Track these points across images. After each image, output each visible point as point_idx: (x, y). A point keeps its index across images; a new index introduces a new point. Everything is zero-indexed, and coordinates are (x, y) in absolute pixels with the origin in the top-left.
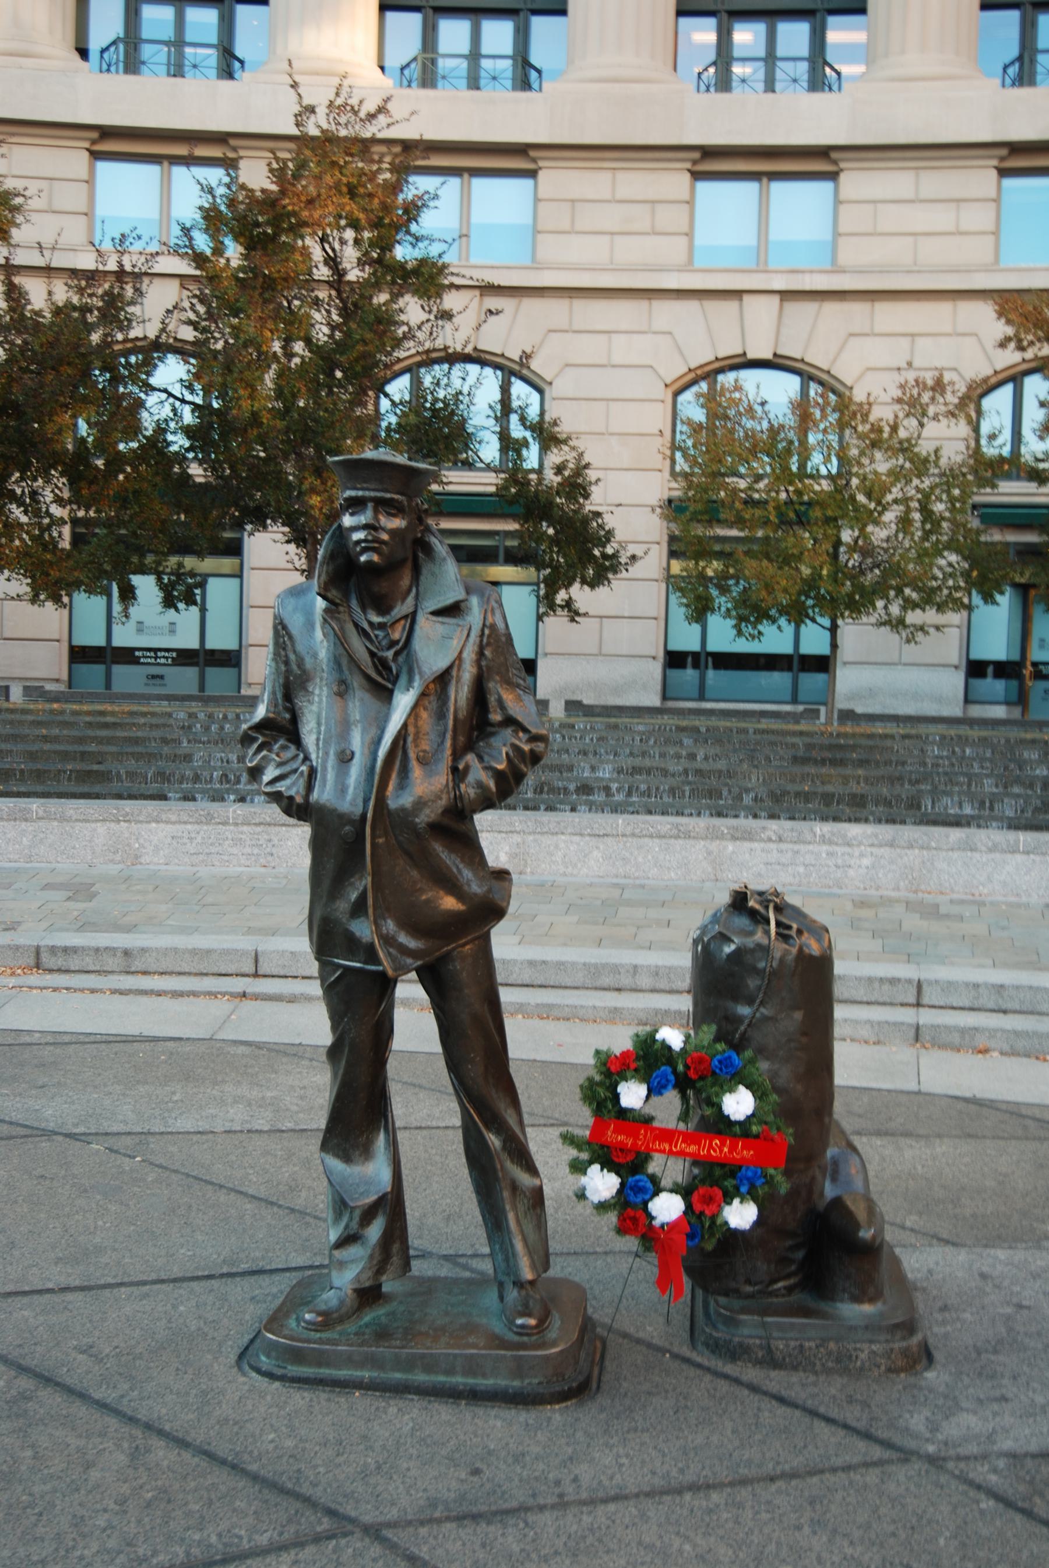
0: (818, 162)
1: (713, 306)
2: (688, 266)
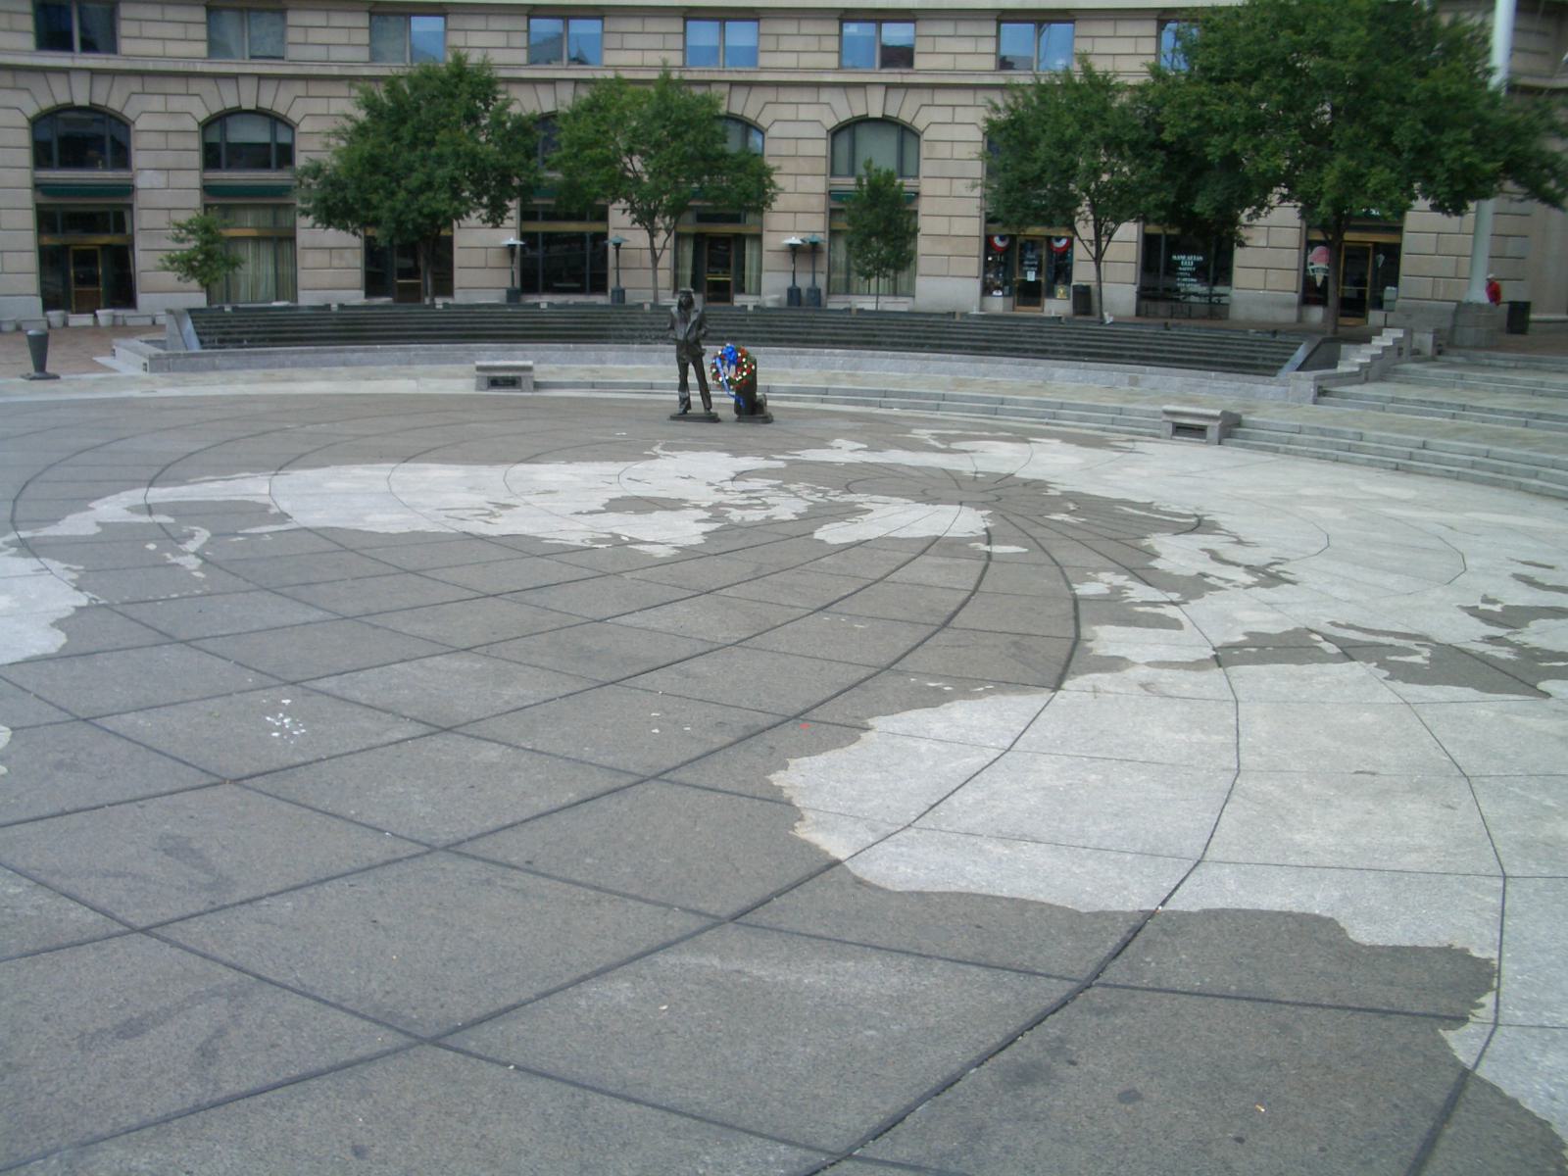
1: (223, 83)
2: (840, 68)
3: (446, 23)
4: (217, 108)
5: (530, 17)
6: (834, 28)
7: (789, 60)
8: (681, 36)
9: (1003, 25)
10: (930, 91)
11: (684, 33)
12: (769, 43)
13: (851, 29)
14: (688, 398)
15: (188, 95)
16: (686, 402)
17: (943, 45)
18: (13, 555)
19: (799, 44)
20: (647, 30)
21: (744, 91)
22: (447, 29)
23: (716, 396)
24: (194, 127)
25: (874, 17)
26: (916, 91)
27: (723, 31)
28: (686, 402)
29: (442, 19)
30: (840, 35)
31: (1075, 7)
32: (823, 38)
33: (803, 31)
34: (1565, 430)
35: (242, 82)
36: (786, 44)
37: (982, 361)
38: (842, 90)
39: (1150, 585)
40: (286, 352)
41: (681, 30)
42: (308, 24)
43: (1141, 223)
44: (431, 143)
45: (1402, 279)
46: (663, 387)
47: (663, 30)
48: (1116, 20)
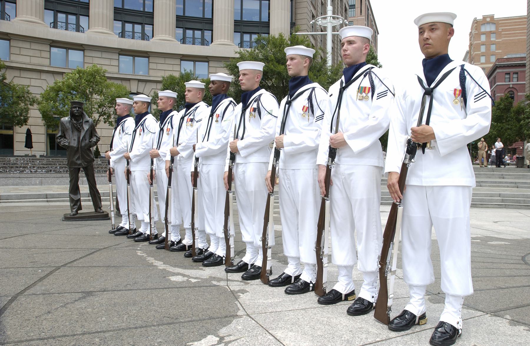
0: (146, 54)
2: (50, 66)
3: (10, 43)
5: (51, 46)
7: (27, 60)
10: (39, 73)
13: (54, 50)
14: (79, 200)
16: (76, 203)
17: (160, 67)
19: (31, 53)
21: (144, 84)
23: (85, 201)
25: (66, 46)
26: (150, 83)
28: (76, 203)
29: (82, 52)
34: (2, 208)
35: (132, 82)
36: (24, 52)
38: (51, 75)
39: (357, 251)
45: (33, 144)
46: (59, 196)
47: (40, 48)
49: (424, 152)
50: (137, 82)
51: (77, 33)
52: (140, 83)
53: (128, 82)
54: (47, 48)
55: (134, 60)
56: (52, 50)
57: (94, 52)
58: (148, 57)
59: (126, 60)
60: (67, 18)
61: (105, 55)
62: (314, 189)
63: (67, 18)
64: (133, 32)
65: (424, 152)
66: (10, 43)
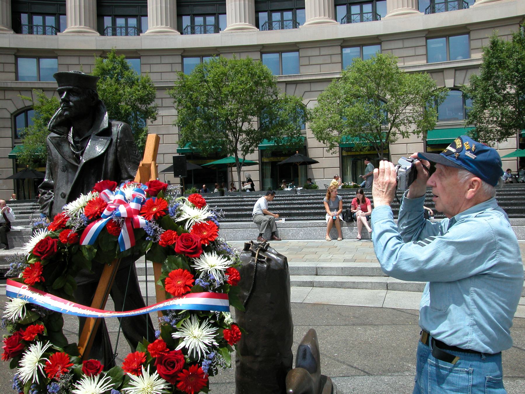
4: (21, 106)
6: (338, 50)
8: (340, 55)
9: (184, 59)
11: (426, 45)
12: (305, 61)
13: (347, 51)
15: (5, 99)
18: (74, 306)
19: (320, 60)
20: (162, 62)
22: (470, 40)
24: (9, 116)
27: (448, 42)
29: (379, 46)
30: (341, 54)
31: (144, 48)
32: (332, 56)
33: (322, 53)
36: (314, 61)
37: (62, 302)
40: (243, 227)
41: (425, 44)
42: (69, 63)
43: (126, 216)
44: (302, 117)
48: (240, 52)
49: (30, 351)
50: (453, 72)
51: (127, 37)
52: (458, 73)
53: (441, 74)
54: (422, 42)
55: (448, 42)
56: (344, 52)
57: (393, 42)
58: (468, 33)
59: (437, 44)
60: (44, 21)
61: (407, 43)
62: (469, 360)
63: (44, 21)
64: (44, 26)
65: (30, 351)
66: (469, 37)
